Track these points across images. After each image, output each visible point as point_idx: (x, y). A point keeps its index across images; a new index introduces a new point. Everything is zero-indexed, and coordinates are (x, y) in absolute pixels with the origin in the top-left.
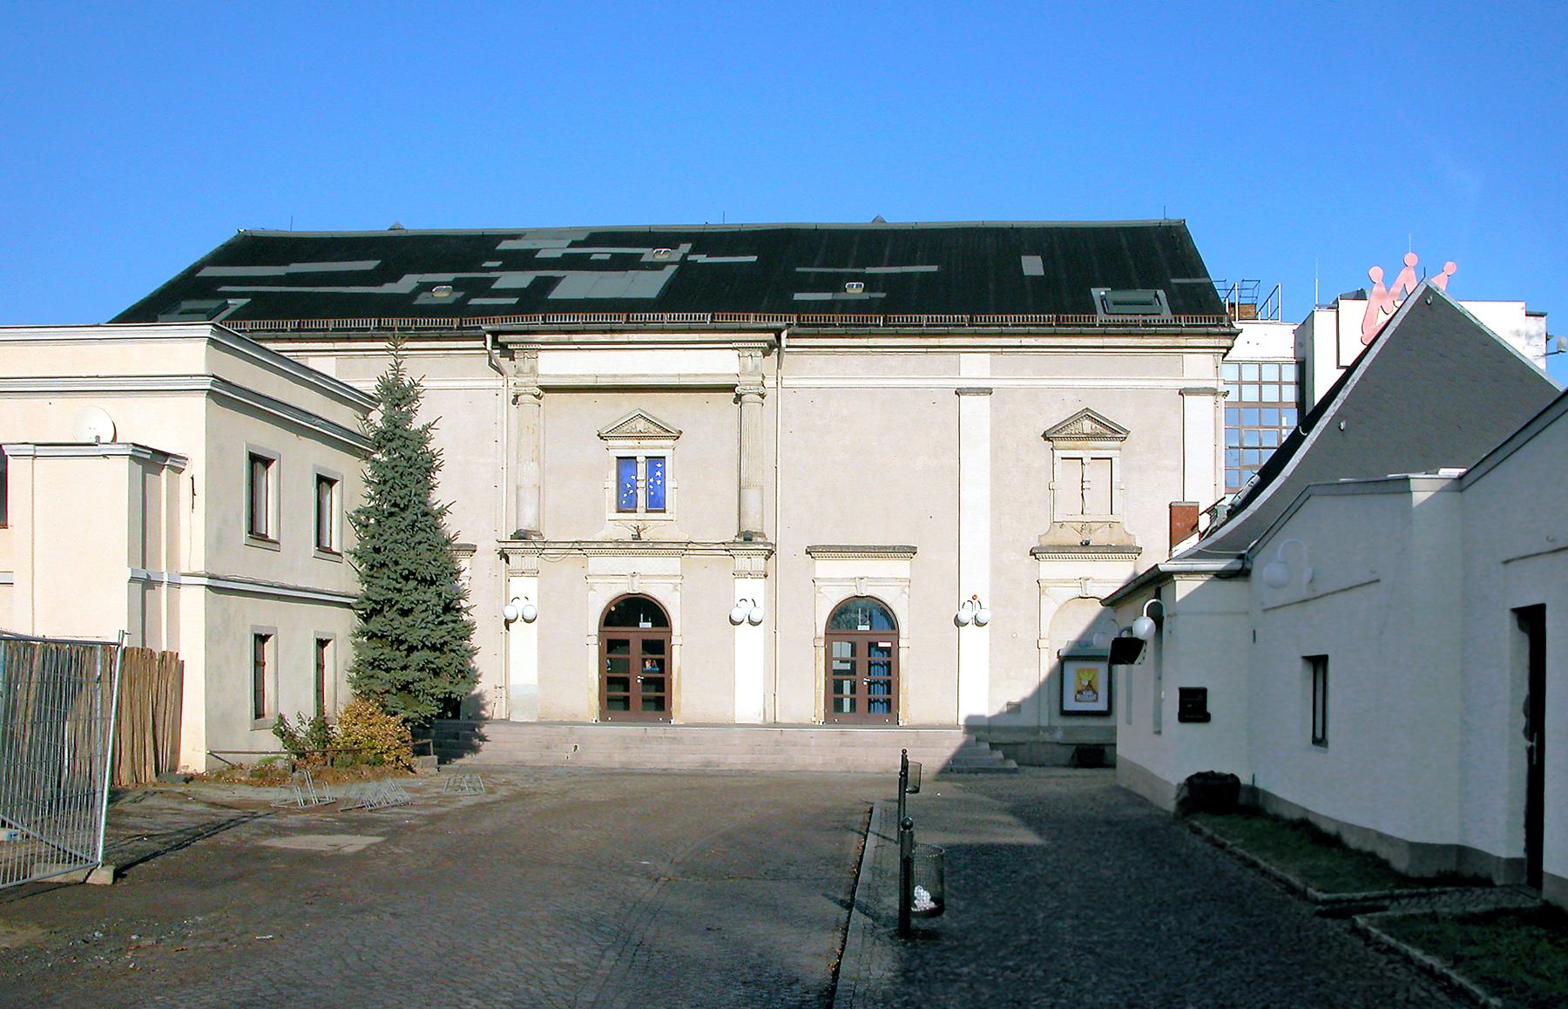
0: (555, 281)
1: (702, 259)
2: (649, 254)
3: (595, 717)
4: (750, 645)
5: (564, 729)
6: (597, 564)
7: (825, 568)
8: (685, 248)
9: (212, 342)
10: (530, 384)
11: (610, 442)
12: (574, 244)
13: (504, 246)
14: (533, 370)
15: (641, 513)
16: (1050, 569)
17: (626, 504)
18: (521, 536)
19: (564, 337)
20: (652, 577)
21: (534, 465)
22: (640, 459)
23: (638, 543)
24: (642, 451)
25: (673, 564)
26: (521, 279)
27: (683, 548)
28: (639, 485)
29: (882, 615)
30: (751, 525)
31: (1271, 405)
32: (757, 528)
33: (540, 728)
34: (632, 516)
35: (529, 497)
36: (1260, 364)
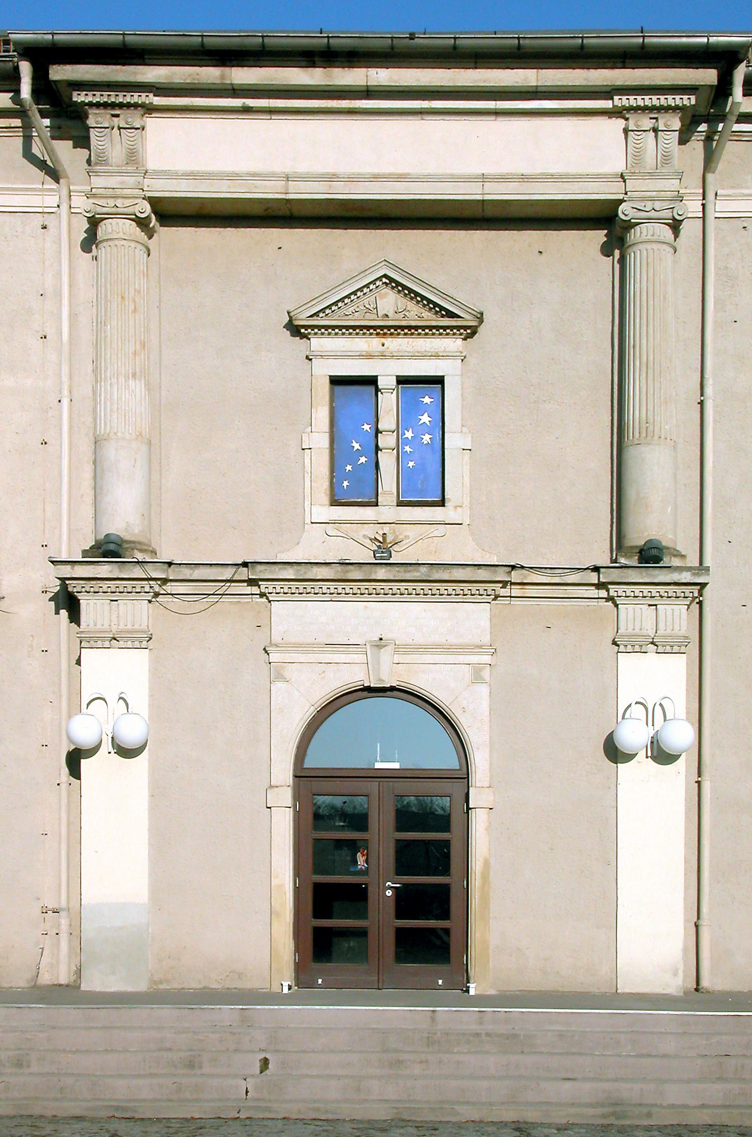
3: (286, 983)
5: (227, 1012)
6: (292, 617)
10: (130, 193)
11: (318, 343)
14: (133, 158)
15: (387, 511)
17: (352, 487)
18: (108, 549)
19: (210, 74)
20: (432, 643)
21: (137, 387)
22: (386, 382)
23: (382, 573)
24: (391, 360)
25: (472, 619)
27: (497, 581)
28: (377, 439)
33: (166, 1012)
34: (368, 513)
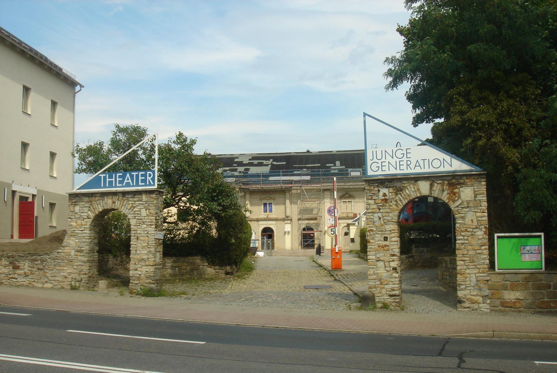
0: (248, 170)
1: (275, 163)
2: (265, 162)
4: (288, 238)
6: (260, 222)
8: (271, 160)
12: (249, 160)
13: (236, 160)
15: (268, 213)
16: (300, 222)
17: (265, 211)
25: (274, 222)
26: (242, 169)
27: (276, 220)
30: (288, 214)
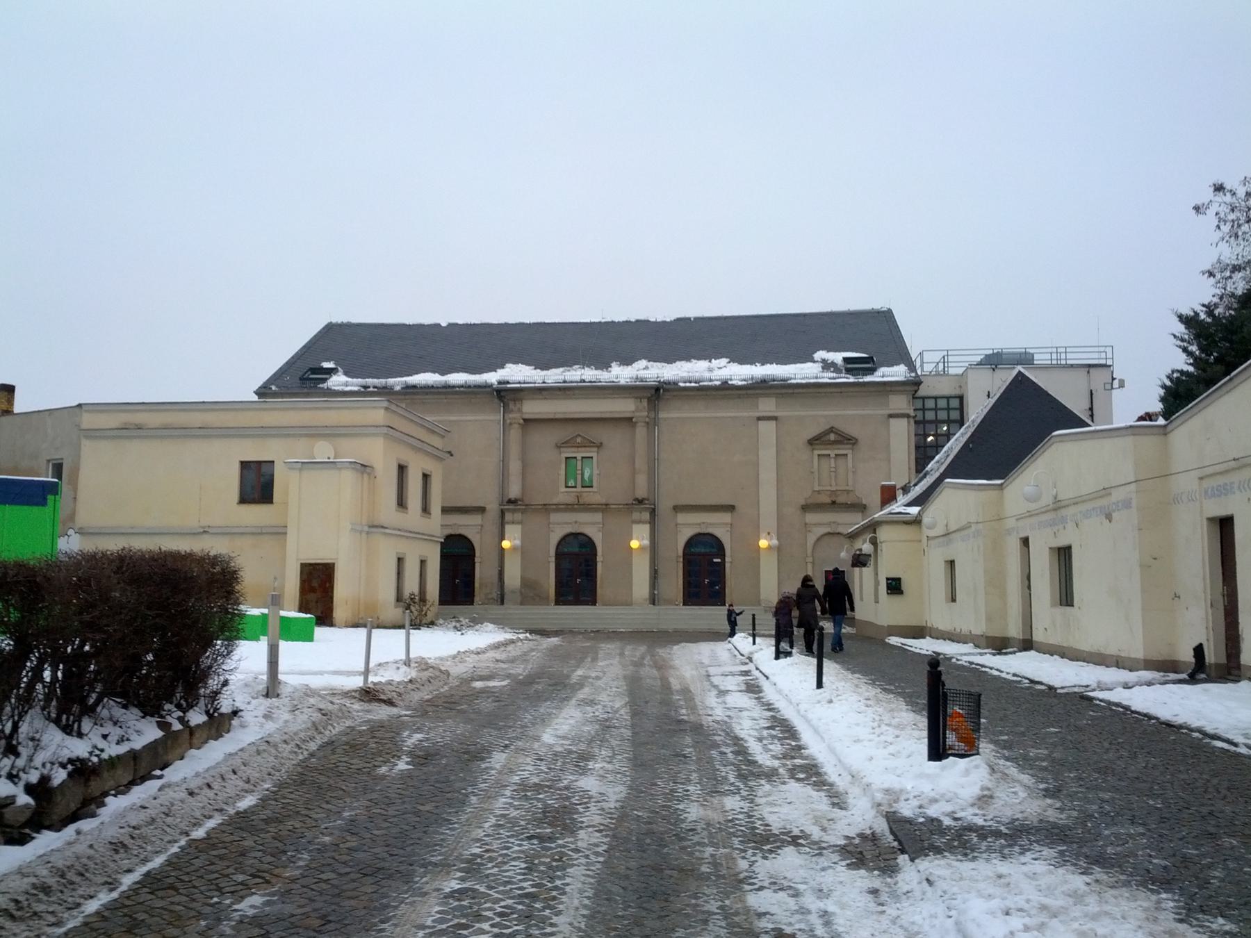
7: (682, 518)
9: (387, 409)
14: (520, 410)
16: (811, 518)
20: (590, 525)
25: (598, 517)
29: (717, 546)
31: (930, 422)
32: (645, 496)
35: (810, 566)
36: (936, 398)
